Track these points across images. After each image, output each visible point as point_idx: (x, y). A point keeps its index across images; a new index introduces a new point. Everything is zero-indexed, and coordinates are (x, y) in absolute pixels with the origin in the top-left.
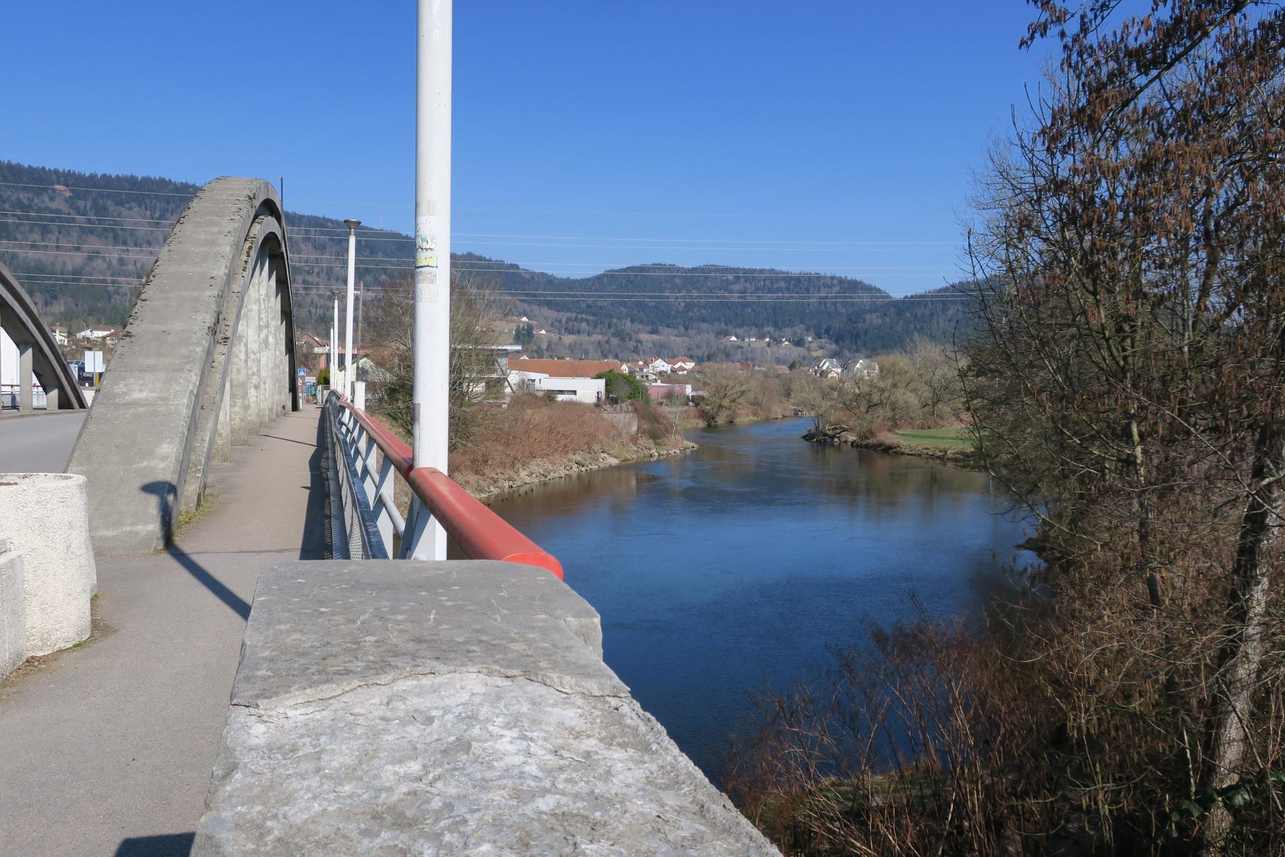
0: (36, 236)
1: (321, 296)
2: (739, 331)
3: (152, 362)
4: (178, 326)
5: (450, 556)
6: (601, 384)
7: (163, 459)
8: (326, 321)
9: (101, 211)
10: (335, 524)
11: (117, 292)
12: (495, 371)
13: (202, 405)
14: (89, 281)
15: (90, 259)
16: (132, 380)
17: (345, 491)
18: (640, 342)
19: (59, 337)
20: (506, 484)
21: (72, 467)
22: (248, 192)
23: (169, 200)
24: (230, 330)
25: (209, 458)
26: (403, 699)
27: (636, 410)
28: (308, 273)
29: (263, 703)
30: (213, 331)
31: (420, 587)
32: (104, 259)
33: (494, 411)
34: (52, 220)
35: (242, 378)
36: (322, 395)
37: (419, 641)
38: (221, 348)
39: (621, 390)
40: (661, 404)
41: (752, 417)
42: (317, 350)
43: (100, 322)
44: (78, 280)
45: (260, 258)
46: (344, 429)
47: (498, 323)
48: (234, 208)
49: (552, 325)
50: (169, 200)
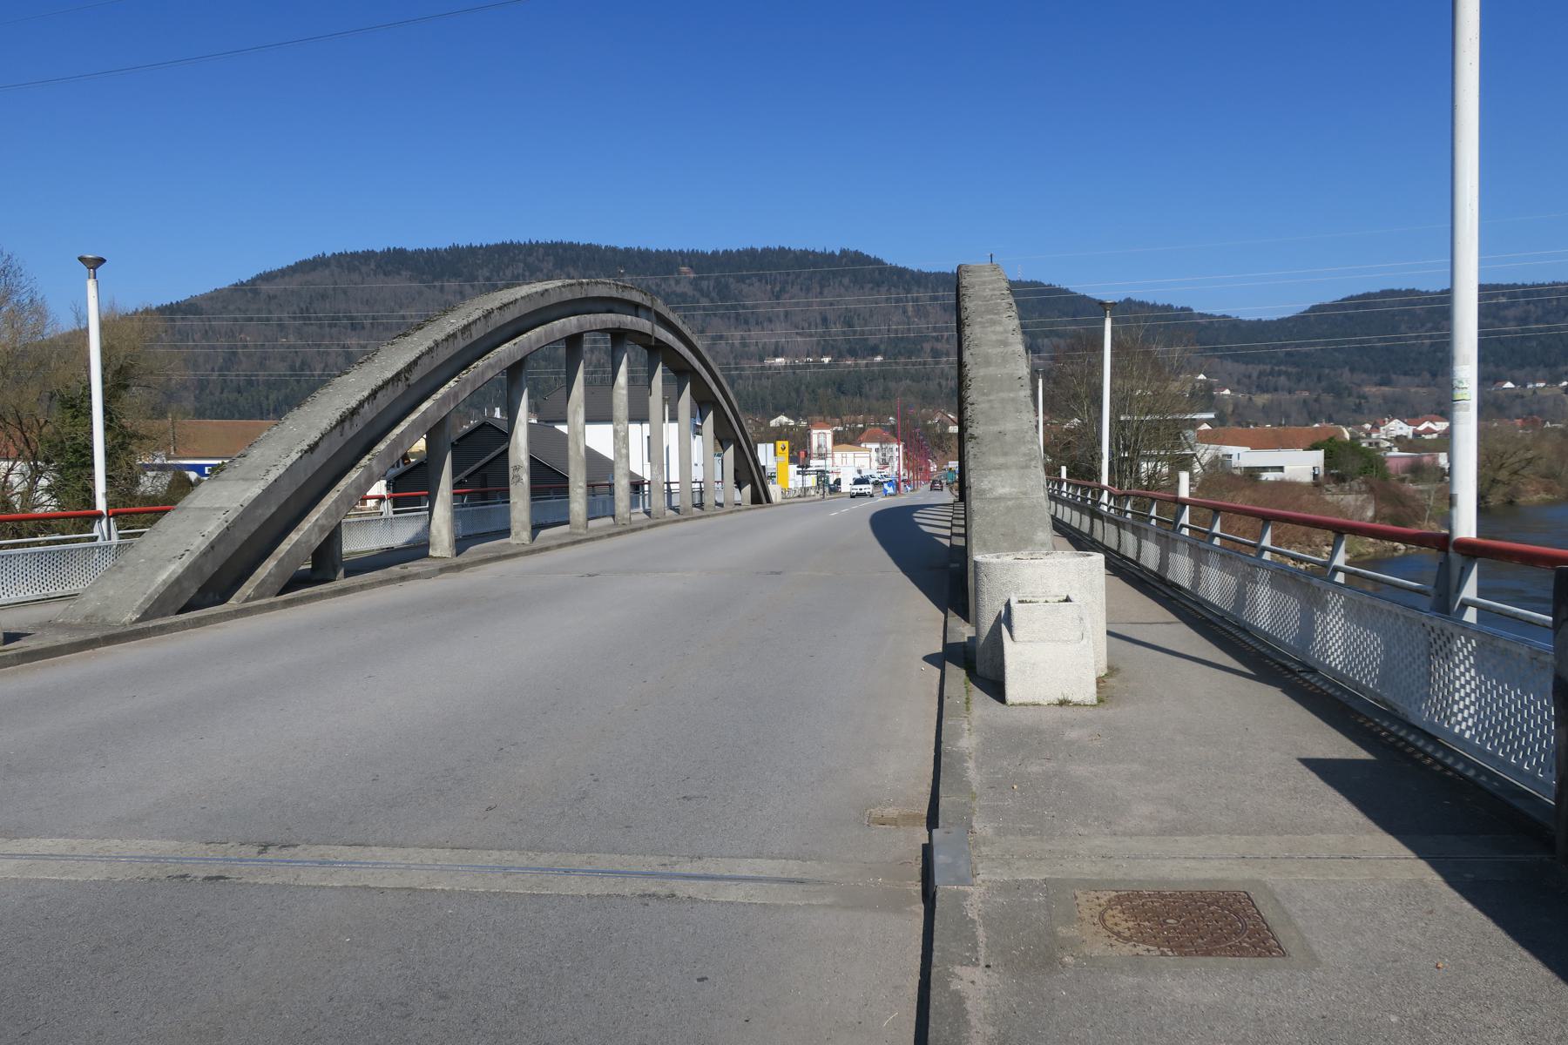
2: (1517, 374)
3: (1001, 460)
6: (1317, 457)
18: (1365, 398)
27: (1371, 490)
28: (937, 339)
39: (1346, 463)
40: (1403, 480)
41: (1543, 495)
49: (1239, 382)
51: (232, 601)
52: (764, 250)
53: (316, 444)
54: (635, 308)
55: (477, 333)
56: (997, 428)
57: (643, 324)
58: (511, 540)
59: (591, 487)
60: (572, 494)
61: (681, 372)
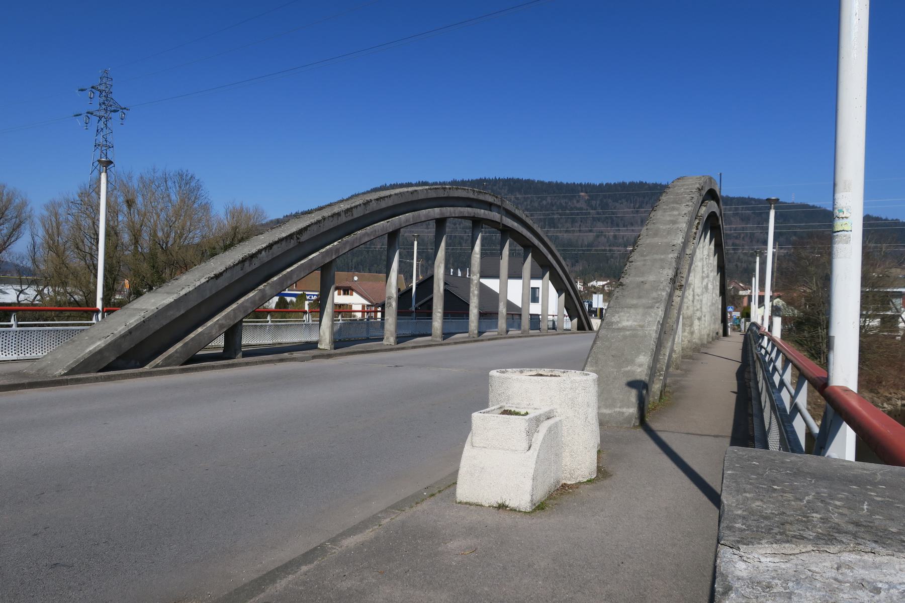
0: (569, 225)
1: (745, 254)
3: (635, 302)
4: (651, 278)
5: (857, 459)
7: (640, 365)
8: (750, 273)
9: (605, 206)
10: (756, 421)
11: (612, 257)
12: (890, 309)
13: (665, 331)
14: (596, 250)
15: (598, 236)
16: (622, 314)
17: (764, 397)
19: (579, 286)
20: (899, 403)
21: (587, 368)
22: (698, 186)
23: (646, 196)
24: (684, 280)
25: (668, 367)
26: (850, 568)
28: (736, 238)
29: (743, 548)
30: (673, 281)
31: (851, 481)
32: (605, 236)
33: (888, 342)
34: (578, 214)
35: (689, 312)
36: (744, 325)
37: (857, 524)
38: (678, 293)
42: (741, 293)
43: (601, 276)
44: (590, 250)
45: (705, 231)
46: (763, 351)
47: (893, 270)
48: (688, 197)
50: (646, 196)
51: (147, 367)
52: (630, 183)
53: (221, 274)
54: (489, 206)
55: (357, 214)
56: (641, 279)
57: (495, 216)
58: (385, 342)
59: (482, 315)
60: (434, 316)
61: (528, 247)
